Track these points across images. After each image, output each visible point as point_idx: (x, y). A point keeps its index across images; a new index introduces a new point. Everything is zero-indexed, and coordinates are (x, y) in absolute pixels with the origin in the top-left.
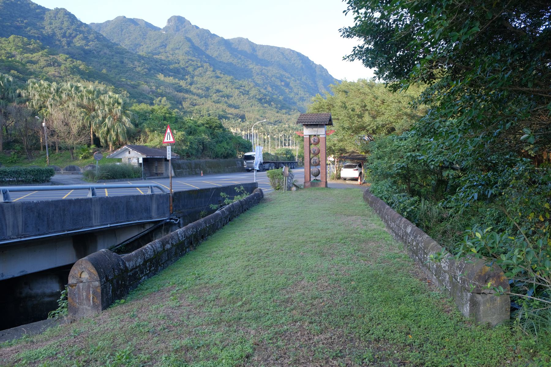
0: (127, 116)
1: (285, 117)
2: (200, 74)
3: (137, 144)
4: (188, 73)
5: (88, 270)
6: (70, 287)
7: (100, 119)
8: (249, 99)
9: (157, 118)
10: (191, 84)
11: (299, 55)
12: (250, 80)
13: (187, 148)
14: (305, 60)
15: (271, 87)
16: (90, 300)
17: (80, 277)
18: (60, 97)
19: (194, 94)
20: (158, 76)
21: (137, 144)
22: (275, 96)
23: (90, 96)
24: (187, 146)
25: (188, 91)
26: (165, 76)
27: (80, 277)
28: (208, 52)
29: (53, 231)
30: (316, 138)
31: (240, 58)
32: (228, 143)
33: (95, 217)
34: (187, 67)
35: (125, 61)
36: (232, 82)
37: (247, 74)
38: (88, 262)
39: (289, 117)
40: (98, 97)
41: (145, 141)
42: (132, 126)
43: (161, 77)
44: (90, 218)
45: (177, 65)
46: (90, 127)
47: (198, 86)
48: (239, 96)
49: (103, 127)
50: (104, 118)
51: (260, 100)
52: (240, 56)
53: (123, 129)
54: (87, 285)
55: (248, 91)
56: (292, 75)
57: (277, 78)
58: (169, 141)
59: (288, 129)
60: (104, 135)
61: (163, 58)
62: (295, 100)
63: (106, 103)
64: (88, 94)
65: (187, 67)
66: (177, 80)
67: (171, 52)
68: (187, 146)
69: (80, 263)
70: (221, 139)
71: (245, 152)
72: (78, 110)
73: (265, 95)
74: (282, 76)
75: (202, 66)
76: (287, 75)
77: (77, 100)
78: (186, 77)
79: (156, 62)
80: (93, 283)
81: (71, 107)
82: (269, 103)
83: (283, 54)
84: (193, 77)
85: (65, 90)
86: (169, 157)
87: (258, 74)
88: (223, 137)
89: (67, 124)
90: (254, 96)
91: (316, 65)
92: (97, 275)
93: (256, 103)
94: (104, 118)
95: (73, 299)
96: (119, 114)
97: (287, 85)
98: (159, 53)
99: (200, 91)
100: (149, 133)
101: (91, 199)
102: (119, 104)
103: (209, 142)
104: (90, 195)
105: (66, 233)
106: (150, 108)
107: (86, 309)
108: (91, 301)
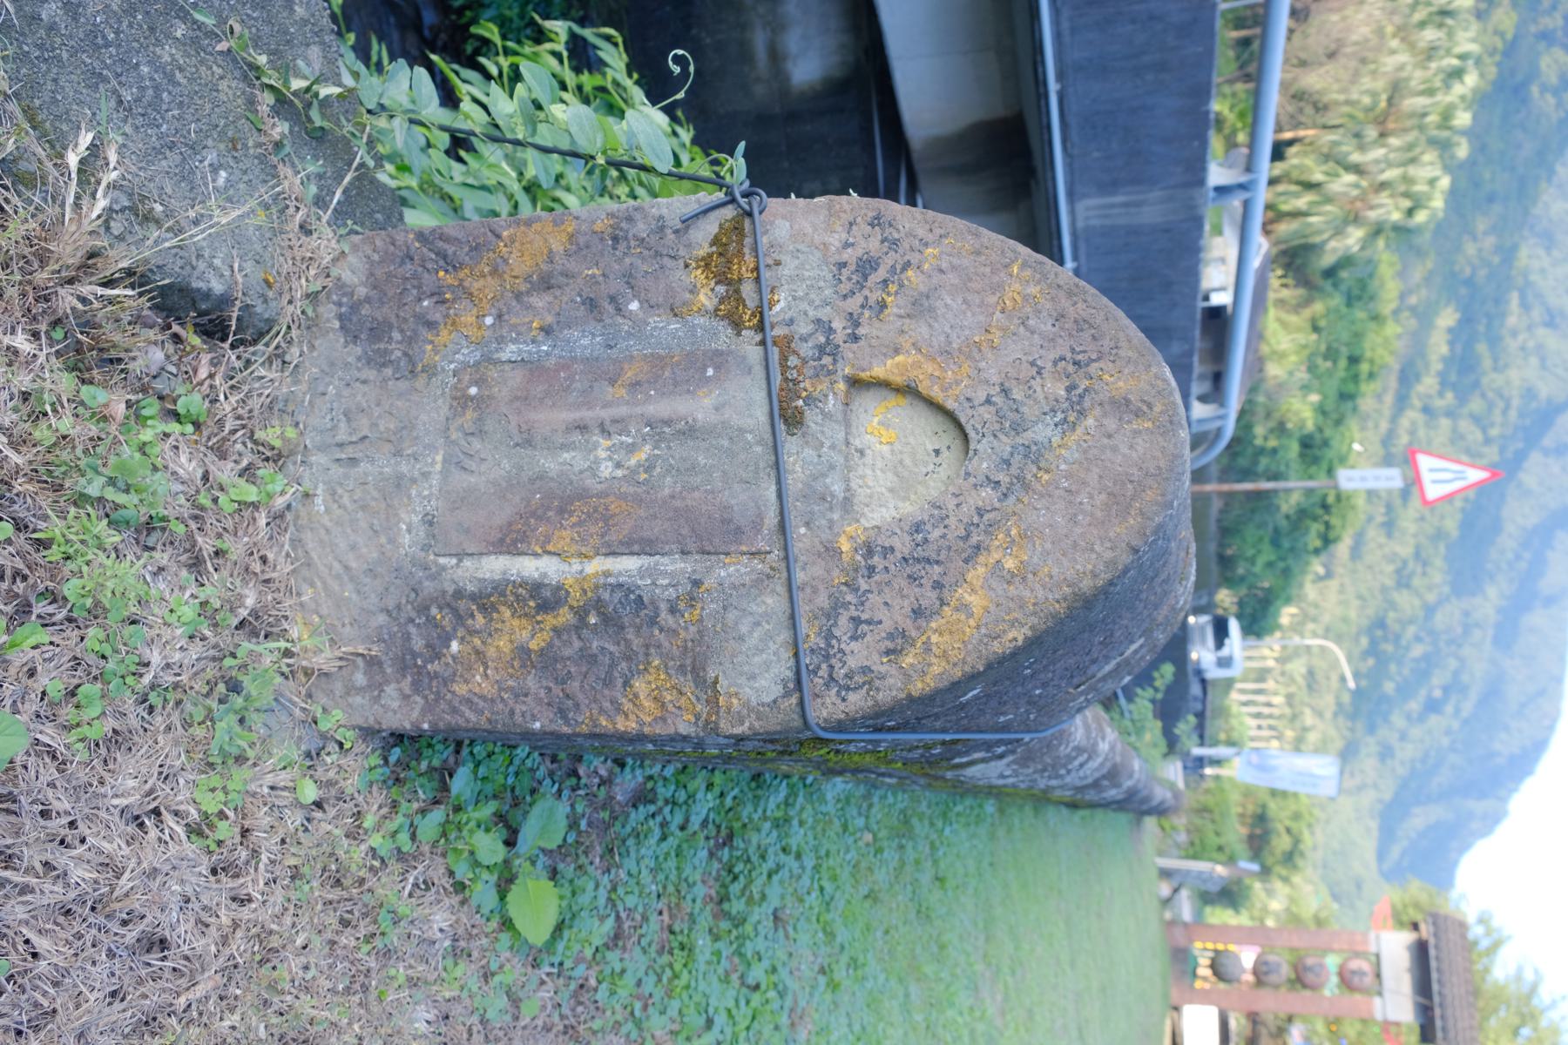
0: (1367, 242)
1: (1328, 701)
2: (1462, 437)
3: (1274, 282)
4: (1462, 399)
5: (984, 523)
6: (709, 227)
7: (1356, 157)
8: (1384, 590)
9: (1358, 336)
10: (1426, 410)
11: (1540, 746)
12: (1446, 589)
13: (1259, 442)
14: (1523, 763)
15: (1426, 657)
16: (510, 542)
17: (855, 383)
18: (1422, 25)
19: (1394, 419)
20: (1449, 310)
21: (1274, 282)
22: (1393, 667)
23: (1432, 119)
24: (1266, 438)
25: (1402, 401)
26: (1450, 330)
27: (855, 383)
28: (1535, 457)
29: (1065, 25)
30: (1368, 980)
31: (1518, 557)
32: (1270, 565)
33: (1112, 206)
34: (1483, 396)
35: (1497, 208)
36: (1439, 535)
37: (1466, 579)
38: (1125, 530)
39: (1328, 715)
40: (1433, 142)
41: (1281, 303)
42: (1327, 260)
43: (1447, 318)
44: (1109, 186)
45: (1487, 363)
46: (1325, 127)
47: (1421, 433)
48: (1391, 559)
49: (1324, 168)
50: (1357, 169)
51: (1380, 623)
52: (1527, 555)
53: (1319, 232)
54: (737, 499)
55: (1408, 586)
56: (1466, 722)
57: (1456, 674)
58: (1426, 477)
59: (1298, 724)
60: (1295, 175)
61: (1512, 320)
62: (1383, 732)
63: (1412, 171)
64: (1440, 109)
65: (1483, 396)
66: (1437, 366)
67: (1531, 344)
68: (1266, 438)
69: (1116, 381)
70: (1286, 544)
71: (1239, 617)
72: (1380, 84)
73: (1398, 637)
74: (1463, 690)
75: (1488, 441)
76: (1468, 707)
77: (1417, 77)
78: (1450, 396)
79: (1497, 301)
80: (773, 602)
81: (1390, 63)
82: (1373, 650)
83: (1542, 693)
84: (1450, 414)
85: (1450, 35)
86: (1350, 479)
87: (1467, 614)
88: (1292, 549)
89: (1331, 55)
90: (1393, 605)
91: (1504, 800)
92: (891, 689)
93: (1370, 611)
94: (1357, 169)
95: (546, 284)
96: (1372, 215)
97: (1433, 707)
98: (1525, 306)
99: (1404, 439)
100: (1307, 313)
101: (1201, 181)
102: (1410, 212)
103: (1278, 508)
104: (1217, 175)
105: (1053, 87)
106: (1387, 309)
107: (400, 482)
108: (495, 566)
